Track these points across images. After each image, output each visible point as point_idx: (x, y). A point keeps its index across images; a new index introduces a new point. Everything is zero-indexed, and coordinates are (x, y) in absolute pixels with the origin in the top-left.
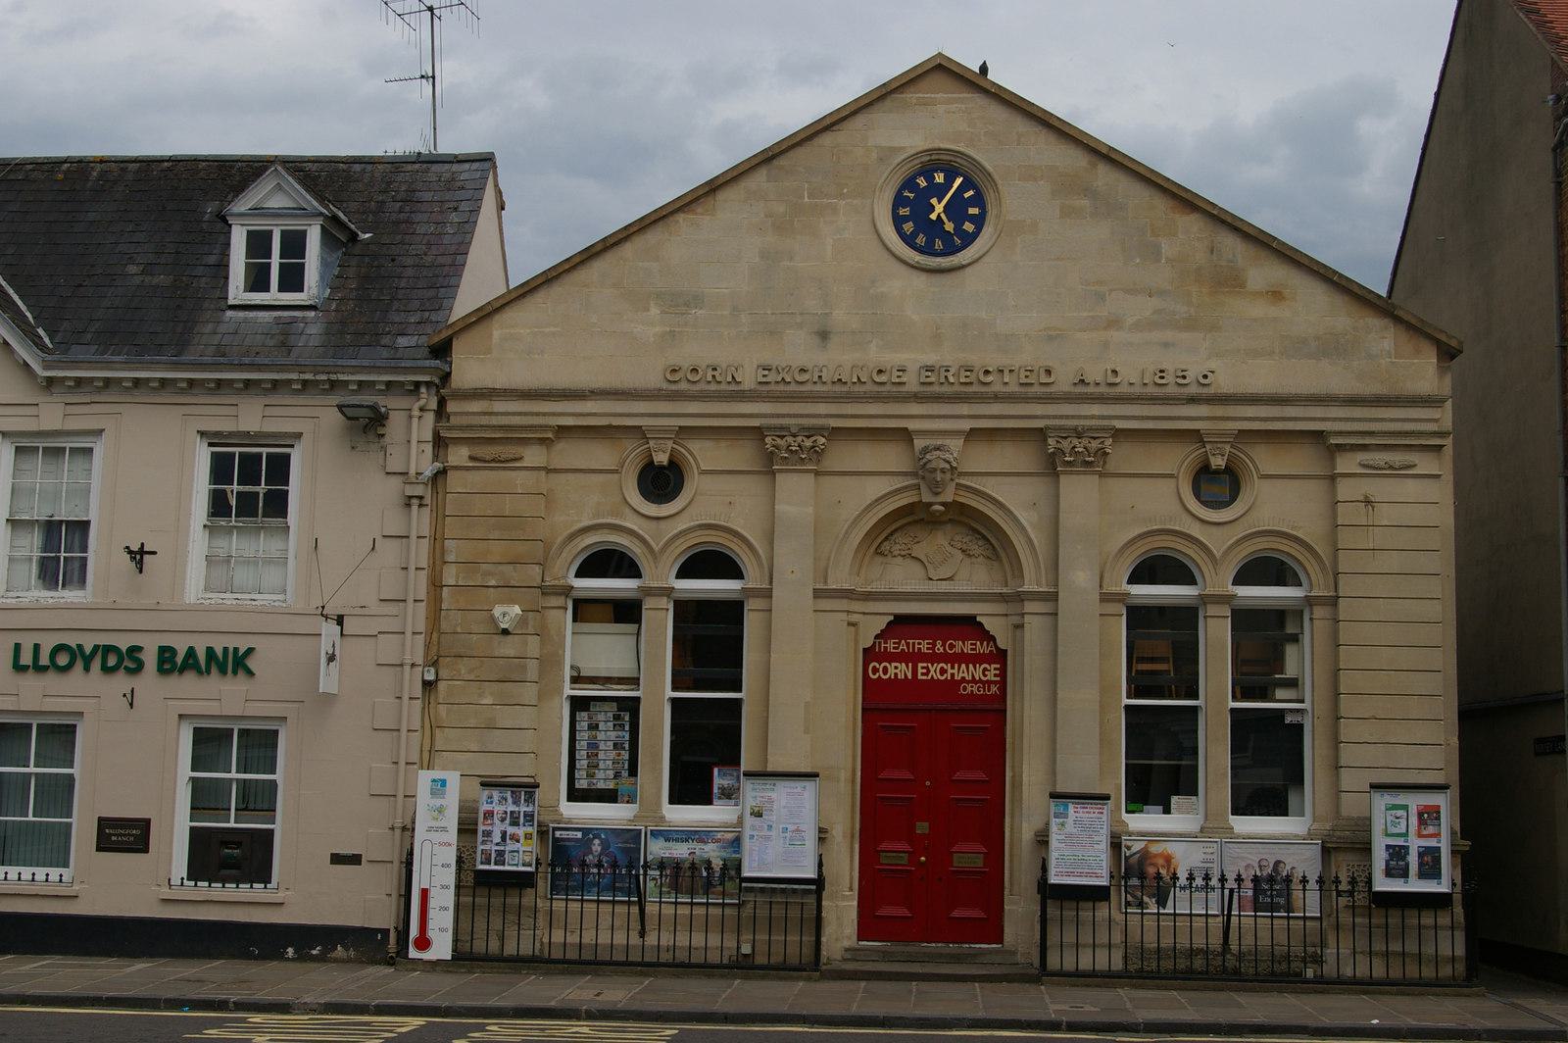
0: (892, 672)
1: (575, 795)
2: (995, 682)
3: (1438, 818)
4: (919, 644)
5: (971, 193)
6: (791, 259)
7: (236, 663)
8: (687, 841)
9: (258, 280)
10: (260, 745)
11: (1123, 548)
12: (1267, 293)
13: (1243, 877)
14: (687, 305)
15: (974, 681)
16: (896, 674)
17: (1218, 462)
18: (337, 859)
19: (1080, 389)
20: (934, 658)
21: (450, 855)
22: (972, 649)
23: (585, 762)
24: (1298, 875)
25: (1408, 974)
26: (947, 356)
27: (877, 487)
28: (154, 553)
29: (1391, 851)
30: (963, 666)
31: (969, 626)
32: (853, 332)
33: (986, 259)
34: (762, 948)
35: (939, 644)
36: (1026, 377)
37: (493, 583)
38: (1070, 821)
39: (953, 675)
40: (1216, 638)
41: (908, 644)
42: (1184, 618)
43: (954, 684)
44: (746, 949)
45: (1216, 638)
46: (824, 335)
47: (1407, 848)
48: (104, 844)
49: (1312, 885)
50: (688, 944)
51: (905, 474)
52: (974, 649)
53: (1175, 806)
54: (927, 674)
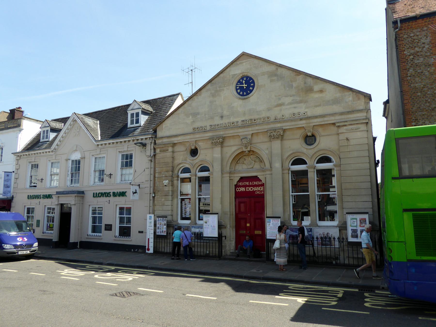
0: (241, 189)
1: (183, 218)
2: (263, 191)
3: (366, 221)
4: (246, 183)
5: (251, 81)
6: (215, 102)
7: (123, 194)
8: (198, 228)
9: (132, 123)
10: (129, 210)
11: (287, 157)
12: (319, 91)
13: (318, 237)
14: (196, 115)
15: (258, 191)
16: (242, 190)
17: (309, 134)
18: (140, 232)
19: (276, 121)
20: (249, 186)
21: (152, 232)
22: (257, 184)
23: (184, 212)
24: (333, 236)
25: (350, 263)
26: (247, 118)
27: (234, 149)
28: (112, 175)
29: (352, 230)
30: (256, 187)
31: (256, 178)
32: (228, 116)
33: (254, 95)
34: (211, 252)
35: (251, 183)
36: (263, 120)
37: (164, 176)
38: (271, 223)
39: (254, 190)
40: (313, 178)
41: (244, 183)
42: (305, 173)
43: (254, 192)
44: (208, 252)
45: (313, 178)
46: (222, 117)
47: (357, 230)
48: (106, 229)
49: (336, 240)
50: (197, 251)
51: (240, 145)
52: (258, 183)
53: (305, 219)
54: (248, 190)
